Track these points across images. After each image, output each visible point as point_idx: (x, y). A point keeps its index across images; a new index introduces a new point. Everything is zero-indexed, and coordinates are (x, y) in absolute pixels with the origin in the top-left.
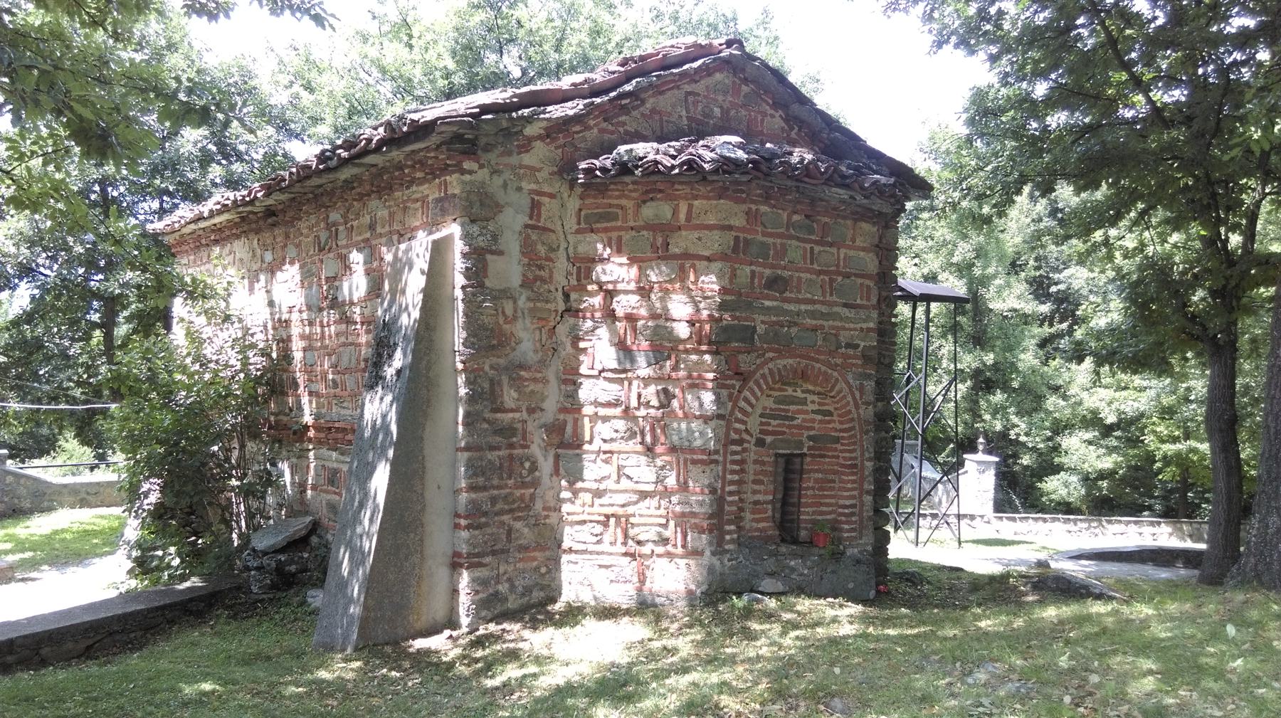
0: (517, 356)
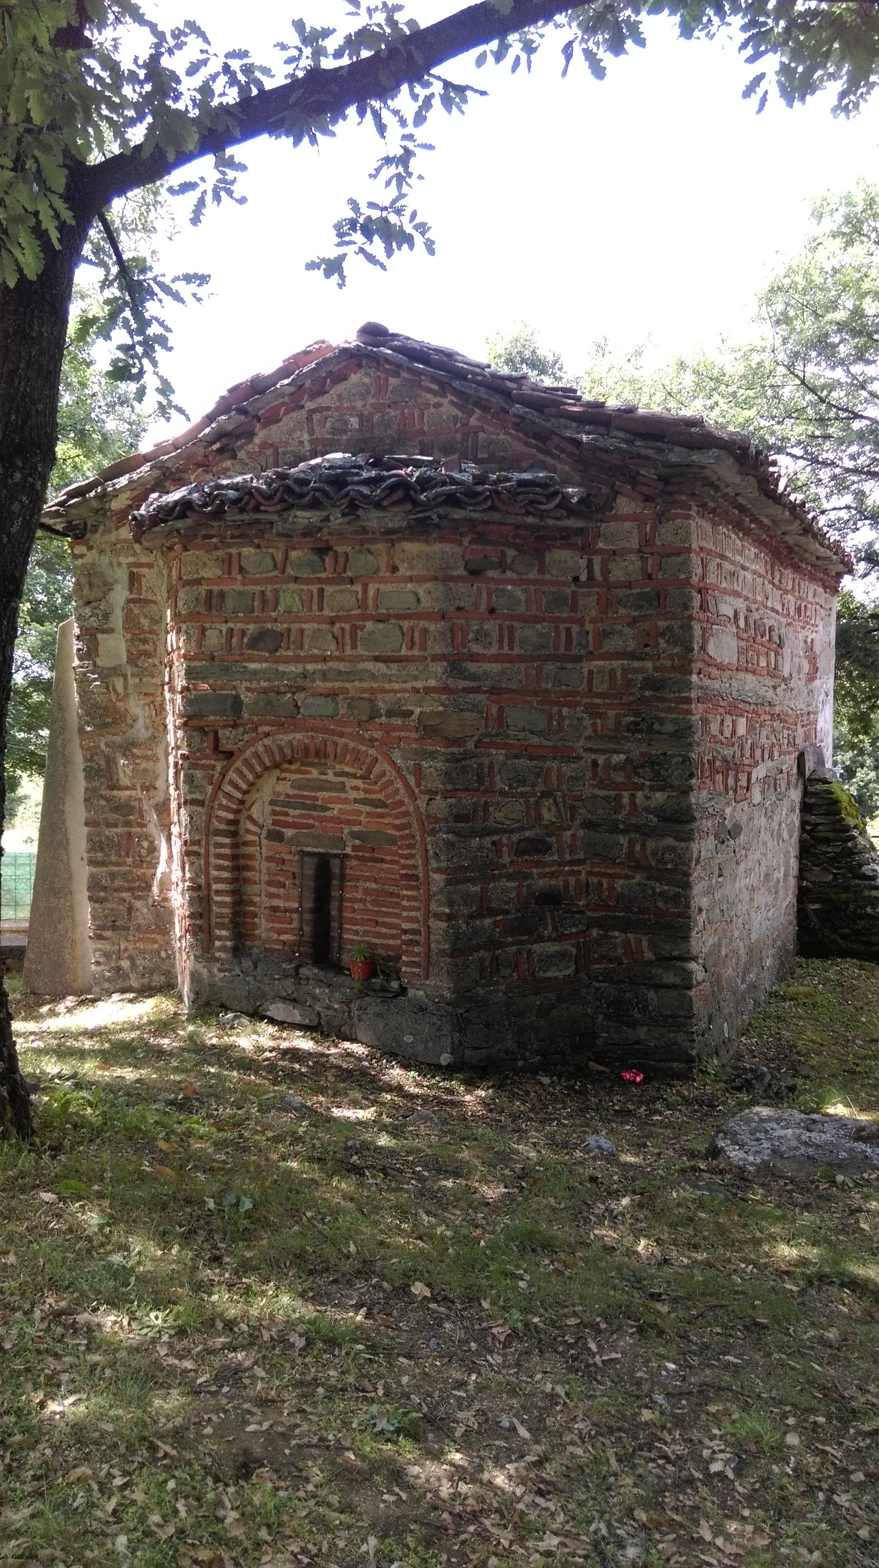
0: (131, 733)
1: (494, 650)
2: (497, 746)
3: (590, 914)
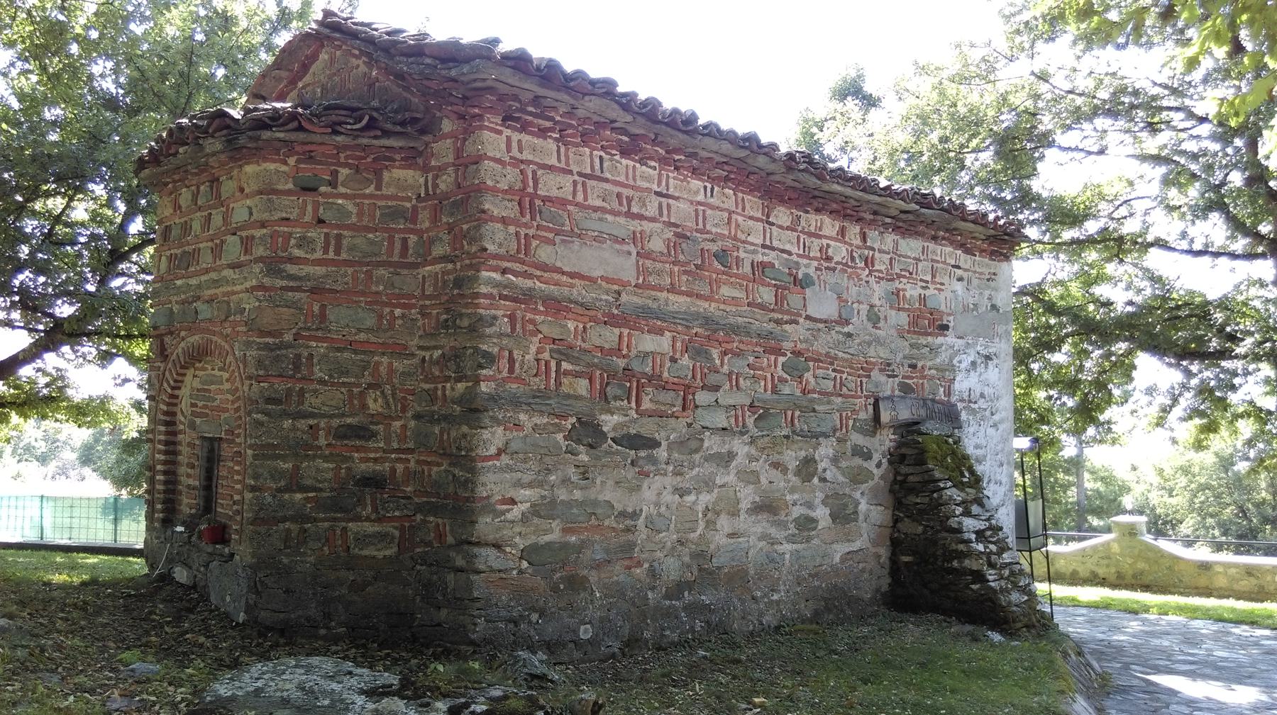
1: (318, 255)
2: (317, 339)
3: (416, 500)
